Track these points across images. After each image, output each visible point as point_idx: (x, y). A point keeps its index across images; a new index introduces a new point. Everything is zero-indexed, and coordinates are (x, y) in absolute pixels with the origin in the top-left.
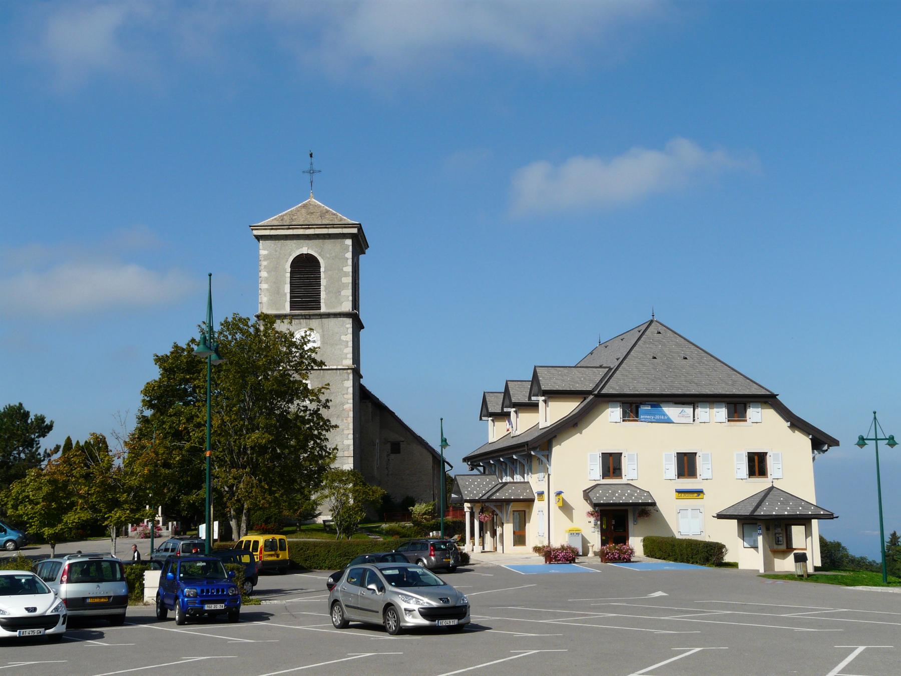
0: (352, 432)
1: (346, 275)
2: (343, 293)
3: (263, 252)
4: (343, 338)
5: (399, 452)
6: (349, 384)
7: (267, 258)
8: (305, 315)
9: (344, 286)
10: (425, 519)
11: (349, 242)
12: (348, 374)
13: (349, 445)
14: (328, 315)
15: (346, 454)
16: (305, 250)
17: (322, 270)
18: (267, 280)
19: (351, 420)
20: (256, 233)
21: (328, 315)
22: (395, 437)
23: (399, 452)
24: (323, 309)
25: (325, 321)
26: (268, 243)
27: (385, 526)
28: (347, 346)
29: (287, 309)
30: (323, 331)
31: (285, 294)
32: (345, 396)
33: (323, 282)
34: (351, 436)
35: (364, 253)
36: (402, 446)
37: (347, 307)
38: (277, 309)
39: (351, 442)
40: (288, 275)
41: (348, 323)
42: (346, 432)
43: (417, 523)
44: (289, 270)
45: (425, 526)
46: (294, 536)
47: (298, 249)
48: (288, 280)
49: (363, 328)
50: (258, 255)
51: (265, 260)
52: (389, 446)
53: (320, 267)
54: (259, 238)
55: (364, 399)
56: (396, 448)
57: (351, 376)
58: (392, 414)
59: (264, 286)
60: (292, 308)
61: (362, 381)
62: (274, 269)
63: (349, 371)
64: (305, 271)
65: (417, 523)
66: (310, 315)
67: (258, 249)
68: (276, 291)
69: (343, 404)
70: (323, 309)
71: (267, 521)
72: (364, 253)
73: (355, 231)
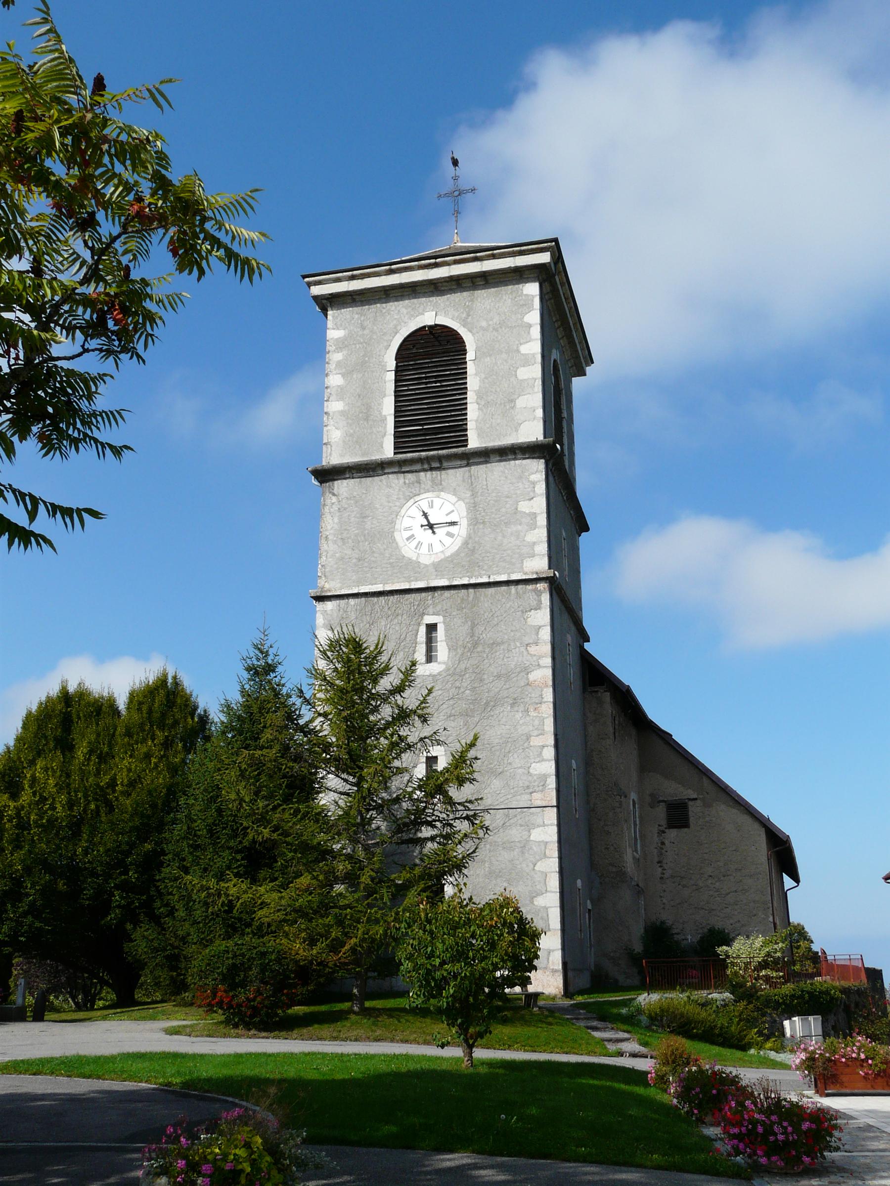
0: (551, 741)
1: (527, 361)
2: (521, 402)
3: (333, 334)
4: (524, 507)
5: (686, 825)
6: (542, 617)
7: (341, 344)
8: (428, 459)
9: (523, 387)
10: (767, 979)
11: (532, 289)
12: (539, 593)
13: (544, 777)
14: (485, 455)
15: (538, 799)
16: (429, 318)
17: (470, 356)
18: (341, 393)
19: (547, 710)
20: (316, 290)
21: (485, 455)
22: (674, 790)
23: (686, 825)
24: (474, 442)
25: (480, 471)
26: (347, 313)
27: (647, 999)
28: (533, 526)
29: (388, 451)
30: (474, 495)
31: (384, 419)
32: (532, 649)
33: (473, 382)
34: (550, 753)
35: (584, 374)
36: (694, 809)
37: (533, 431)
38: (363, 455)
39: (549, 767)
40: (391, 376)
41: (535, 471)
42: (536, 742)
43: (744, 993)
44: (392, 364)
45: (768, 1002)
46: (326, 1030)
47: (412, 316)
48: (391, 387)
49: (586, 529)
50: (322, 339)
51: (339, 349)
52: (661, 812)
53: (464, 351)
54: (326, 303)
55: (600, 710)
56: (678, 815)
57: (546, 599)
58: (665, 738)
59: (334, 406)
60: (398, 448)
61: (587, 646)
62: (359, 367)
63: (542, 586)
64: (431, 360)
65: (744, 993)
66: (440, 459)
67: (325, 328)
68: (364, 414)
69: (527, 670)
70: (474, 442)
71: (234, 976)
72: (584, 374)
73: (544, 258)
